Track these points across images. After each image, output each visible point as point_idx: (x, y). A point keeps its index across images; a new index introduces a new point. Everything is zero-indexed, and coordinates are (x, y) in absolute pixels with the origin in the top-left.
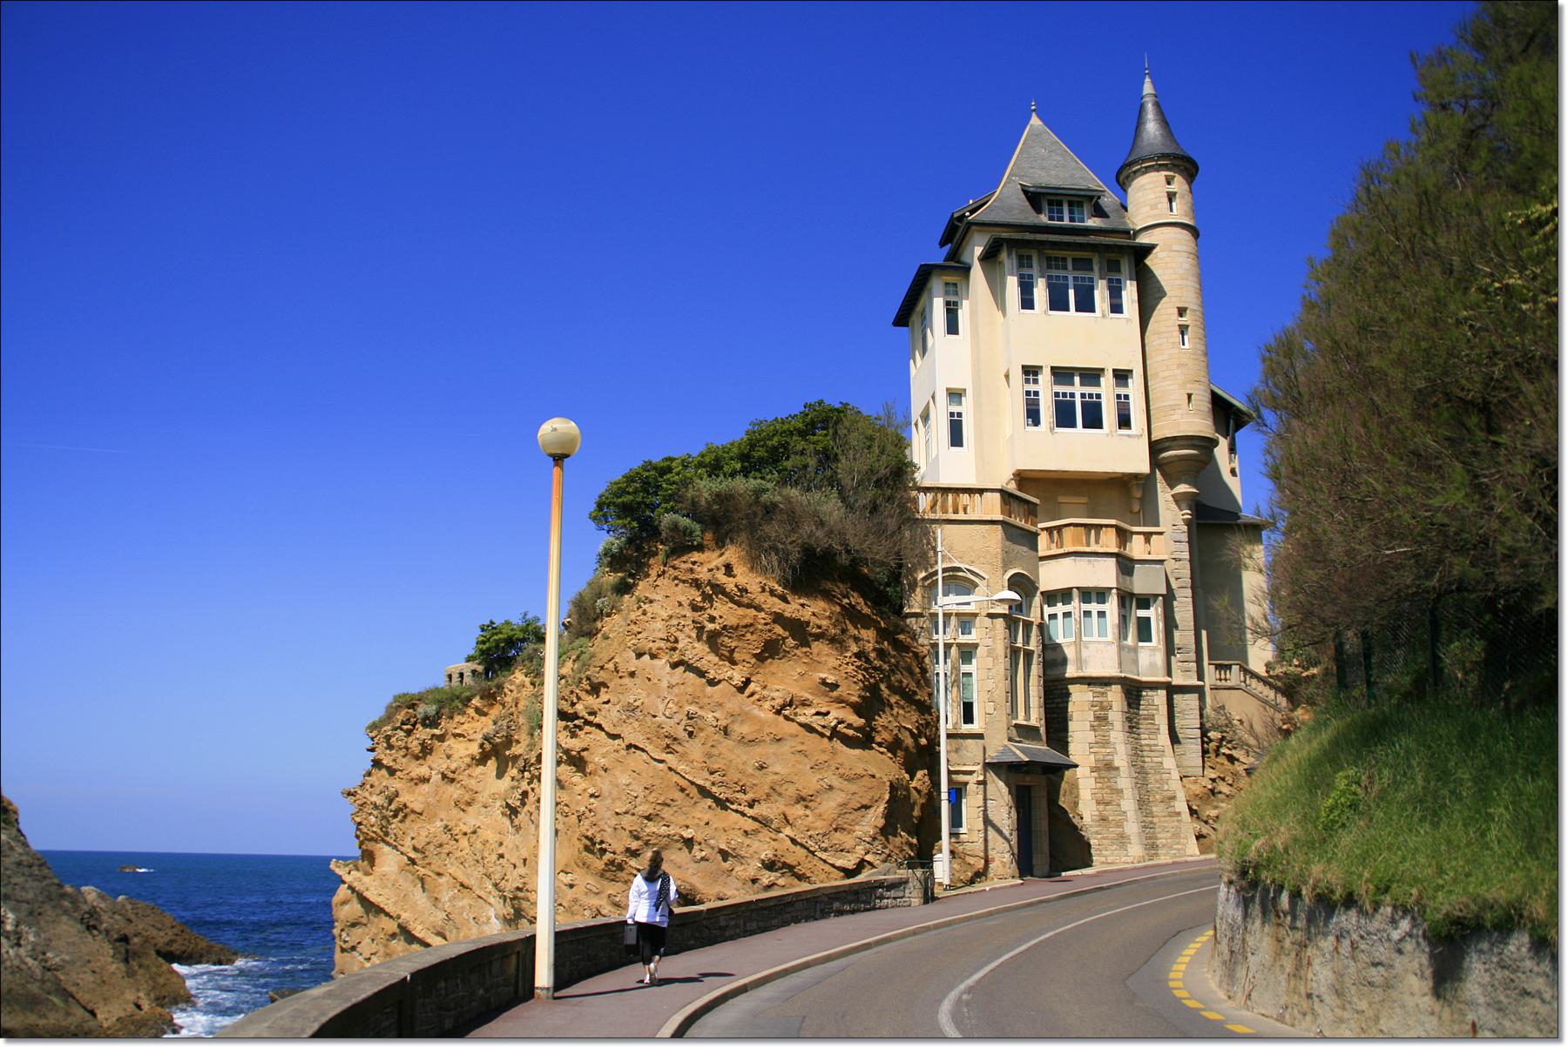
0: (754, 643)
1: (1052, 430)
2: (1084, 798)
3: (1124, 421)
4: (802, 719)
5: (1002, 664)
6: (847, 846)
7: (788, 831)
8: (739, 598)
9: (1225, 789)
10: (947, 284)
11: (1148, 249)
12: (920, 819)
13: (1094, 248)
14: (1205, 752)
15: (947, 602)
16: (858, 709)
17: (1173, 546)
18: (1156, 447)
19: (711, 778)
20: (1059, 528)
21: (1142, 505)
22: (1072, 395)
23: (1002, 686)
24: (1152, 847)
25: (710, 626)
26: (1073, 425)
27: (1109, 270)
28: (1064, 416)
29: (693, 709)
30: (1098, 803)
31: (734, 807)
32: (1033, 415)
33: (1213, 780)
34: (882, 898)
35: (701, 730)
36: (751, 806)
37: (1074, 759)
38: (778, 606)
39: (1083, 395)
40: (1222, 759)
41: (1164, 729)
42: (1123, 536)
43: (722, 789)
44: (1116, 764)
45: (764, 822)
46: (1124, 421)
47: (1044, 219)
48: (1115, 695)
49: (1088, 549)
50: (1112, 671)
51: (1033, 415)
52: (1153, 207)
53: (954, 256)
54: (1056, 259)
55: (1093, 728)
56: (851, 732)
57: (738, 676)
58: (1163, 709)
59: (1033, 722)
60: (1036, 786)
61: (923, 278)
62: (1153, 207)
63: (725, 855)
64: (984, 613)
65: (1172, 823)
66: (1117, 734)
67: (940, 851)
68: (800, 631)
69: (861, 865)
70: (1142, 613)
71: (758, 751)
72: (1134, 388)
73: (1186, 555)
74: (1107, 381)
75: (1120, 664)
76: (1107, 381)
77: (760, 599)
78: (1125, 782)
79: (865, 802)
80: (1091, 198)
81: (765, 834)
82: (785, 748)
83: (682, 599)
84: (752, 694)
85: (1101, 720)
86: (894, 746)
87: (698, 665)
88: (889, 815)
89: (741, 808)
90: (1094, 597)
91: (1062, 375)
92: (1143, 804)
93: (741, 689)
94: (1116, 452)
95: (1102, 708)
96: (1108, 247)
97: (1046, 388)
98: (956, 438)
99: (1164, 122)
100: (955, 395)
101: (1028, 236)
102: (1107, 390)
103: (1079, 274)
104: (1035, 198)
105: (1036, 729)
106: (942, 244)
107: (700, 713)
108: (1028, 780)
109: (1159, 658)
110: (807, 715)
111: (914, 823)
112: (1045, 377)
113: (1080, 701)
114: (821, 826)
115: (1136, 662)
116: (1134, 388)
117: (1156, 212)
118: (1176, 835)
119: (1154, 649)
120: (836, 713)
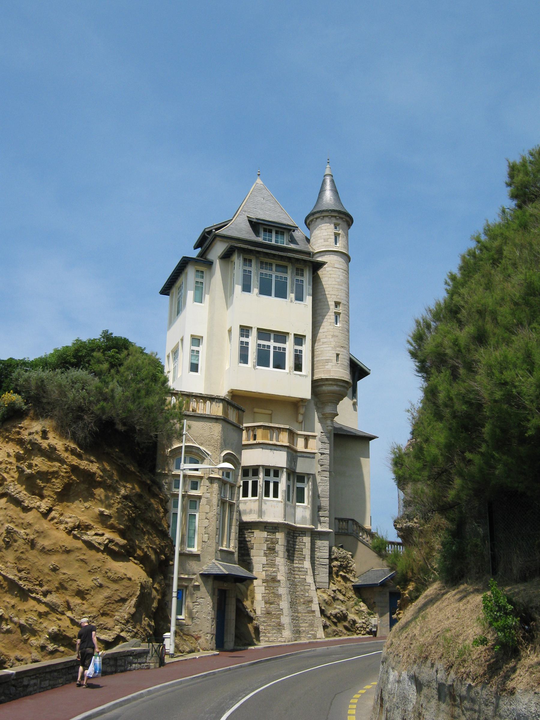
0: (58, 485)
1: (254, 367)
2: (258, 602)
3: (298, 367)
4: (85, 537)
5: (215, 509)
6: (109, 626)
7: (69, 614)
8: (50, 454)
9: (341, 597)
10: (197, 271)
11: (321, 265)
12: (157, 609)
13: (290, 259)
14: (330, 573)
15: (186, 467)
16: (122, 534)
17: (320, 445)
18: (316, 384)
19: (19, 575)
20: (254, 428)
21: (304, 418)
22: (269, 347)
23: (214, 525)
24: (297, 632)
25: (28, 471)
26: (268, 365)
27: (297, 274)
28: (263, 359)
29: (12, 526)
30: (266, 603)
31: (34, 595)
32: (244, 358)
33: (334, 591)
34: (131, 663)
35: (16, 541)
36: (45, 594)
37: (255, 574)
38: (75, 461)
39: (275, 348)
40: (339, 579)
41: (308, 557)
42: (292, 434)
43: (26, 583)
44: (279, 578)
45: (53, 608)
46: (298, 367)
47: (260, 239)
48: (280, 536)
49: (271, 442)
50: (279, 519)
51: (244, 358)
52: (326, 240)
53: (203, 255)
54: (266, 263)
55: (266, 555)
56: (117, 549)
57: (44, 505)
58: (308, 545)
59: (231, 549)
60: (229, 591)
61: (185, 263)
62: (326, 240)
63: (23, 629)
64: (206, 477)
65: (309, 617)
66: (281, 560)
67: (169, 630)
68: (88, 478)
69: (119, 639)
70: (300, 485)
71: (54, 560)
72: (306, 349)
73: (327, 451)
74: (291, 340)
75: (285, 516)
76: (291, 340)
77: (64, 455)
78: (283, 590)
79: (123, 596)
80: (290, 230)
81: (53, 617)
82: (72, 557)
83: (11, 451)
84: (53, 519)
85: (271, 550)
86: (144, 561)
87: (18, 496)
88: (138, 605)
89: (38, 596)
90: (251, 473)
91: (263, 334)
92: (293, 604)
93: (45, 515)
94: (294, 385)
95: (272, 543)
96: (297, 260)
97: (253, 341)
98: (194, 368)
99: (335, 191)
100: (196, 340)
101: (250, 247)
102: (289, 347)
103: (279, 274)
104: (256, 225)
105: (232, 553)
106: (196, 247)
107: (16, 529)
108: (225, 586)
109: (308, 514)
110: (89, 536)
111: (153, 614)
112: (254, 334)
113: (258, 538)
114: (94, 611)
115: (294, 515)
116: (306, 349)
117: (326, 243)
118: (312, 625)
119: (305, 508)
120: (109, 535)
